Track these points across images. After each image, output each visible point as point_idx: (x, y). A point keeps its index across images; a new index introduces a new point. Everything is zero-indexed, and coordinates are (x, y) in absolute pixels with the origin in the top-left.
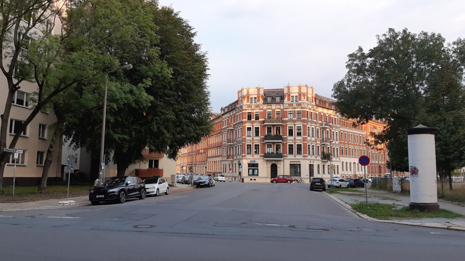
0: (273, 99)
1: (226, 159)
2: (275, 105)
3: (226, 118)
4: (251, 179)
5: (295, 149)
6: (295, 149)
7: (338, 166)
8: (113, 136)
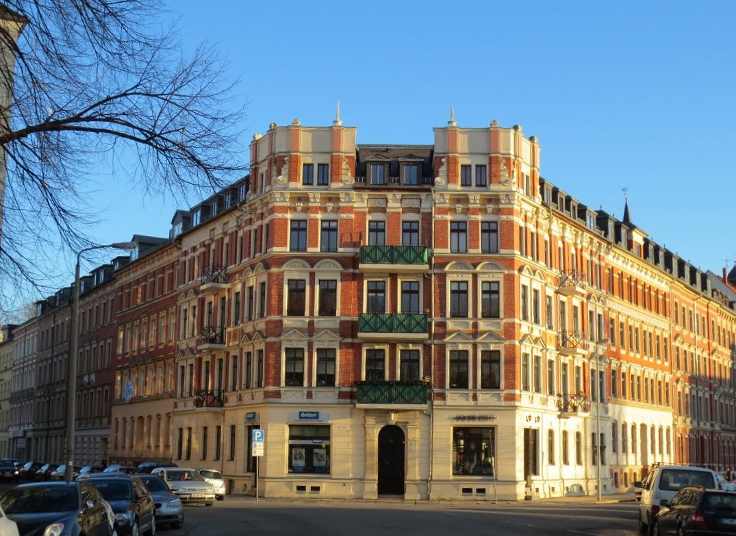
0: (394, 171)
1: (190, 405)
2: (399, 195)
3: (194, 249)
4: (301, 488)
5: (476, 372)
6: (476, 372)
7: (602, 435)
8: (420, 451)
